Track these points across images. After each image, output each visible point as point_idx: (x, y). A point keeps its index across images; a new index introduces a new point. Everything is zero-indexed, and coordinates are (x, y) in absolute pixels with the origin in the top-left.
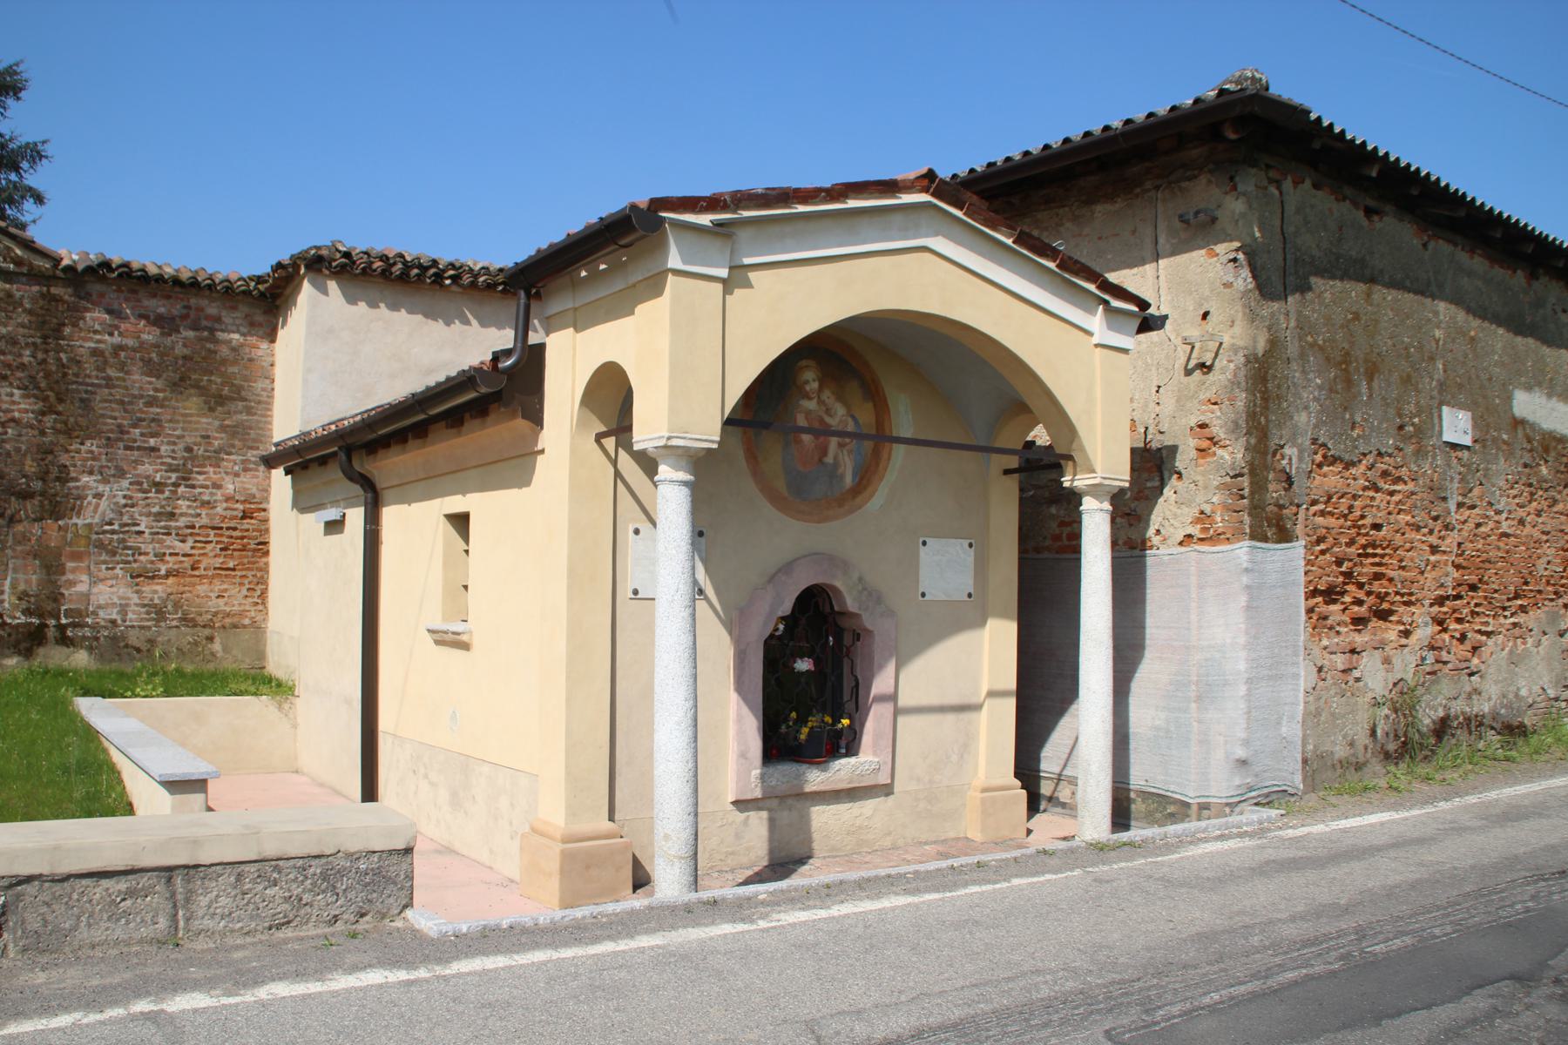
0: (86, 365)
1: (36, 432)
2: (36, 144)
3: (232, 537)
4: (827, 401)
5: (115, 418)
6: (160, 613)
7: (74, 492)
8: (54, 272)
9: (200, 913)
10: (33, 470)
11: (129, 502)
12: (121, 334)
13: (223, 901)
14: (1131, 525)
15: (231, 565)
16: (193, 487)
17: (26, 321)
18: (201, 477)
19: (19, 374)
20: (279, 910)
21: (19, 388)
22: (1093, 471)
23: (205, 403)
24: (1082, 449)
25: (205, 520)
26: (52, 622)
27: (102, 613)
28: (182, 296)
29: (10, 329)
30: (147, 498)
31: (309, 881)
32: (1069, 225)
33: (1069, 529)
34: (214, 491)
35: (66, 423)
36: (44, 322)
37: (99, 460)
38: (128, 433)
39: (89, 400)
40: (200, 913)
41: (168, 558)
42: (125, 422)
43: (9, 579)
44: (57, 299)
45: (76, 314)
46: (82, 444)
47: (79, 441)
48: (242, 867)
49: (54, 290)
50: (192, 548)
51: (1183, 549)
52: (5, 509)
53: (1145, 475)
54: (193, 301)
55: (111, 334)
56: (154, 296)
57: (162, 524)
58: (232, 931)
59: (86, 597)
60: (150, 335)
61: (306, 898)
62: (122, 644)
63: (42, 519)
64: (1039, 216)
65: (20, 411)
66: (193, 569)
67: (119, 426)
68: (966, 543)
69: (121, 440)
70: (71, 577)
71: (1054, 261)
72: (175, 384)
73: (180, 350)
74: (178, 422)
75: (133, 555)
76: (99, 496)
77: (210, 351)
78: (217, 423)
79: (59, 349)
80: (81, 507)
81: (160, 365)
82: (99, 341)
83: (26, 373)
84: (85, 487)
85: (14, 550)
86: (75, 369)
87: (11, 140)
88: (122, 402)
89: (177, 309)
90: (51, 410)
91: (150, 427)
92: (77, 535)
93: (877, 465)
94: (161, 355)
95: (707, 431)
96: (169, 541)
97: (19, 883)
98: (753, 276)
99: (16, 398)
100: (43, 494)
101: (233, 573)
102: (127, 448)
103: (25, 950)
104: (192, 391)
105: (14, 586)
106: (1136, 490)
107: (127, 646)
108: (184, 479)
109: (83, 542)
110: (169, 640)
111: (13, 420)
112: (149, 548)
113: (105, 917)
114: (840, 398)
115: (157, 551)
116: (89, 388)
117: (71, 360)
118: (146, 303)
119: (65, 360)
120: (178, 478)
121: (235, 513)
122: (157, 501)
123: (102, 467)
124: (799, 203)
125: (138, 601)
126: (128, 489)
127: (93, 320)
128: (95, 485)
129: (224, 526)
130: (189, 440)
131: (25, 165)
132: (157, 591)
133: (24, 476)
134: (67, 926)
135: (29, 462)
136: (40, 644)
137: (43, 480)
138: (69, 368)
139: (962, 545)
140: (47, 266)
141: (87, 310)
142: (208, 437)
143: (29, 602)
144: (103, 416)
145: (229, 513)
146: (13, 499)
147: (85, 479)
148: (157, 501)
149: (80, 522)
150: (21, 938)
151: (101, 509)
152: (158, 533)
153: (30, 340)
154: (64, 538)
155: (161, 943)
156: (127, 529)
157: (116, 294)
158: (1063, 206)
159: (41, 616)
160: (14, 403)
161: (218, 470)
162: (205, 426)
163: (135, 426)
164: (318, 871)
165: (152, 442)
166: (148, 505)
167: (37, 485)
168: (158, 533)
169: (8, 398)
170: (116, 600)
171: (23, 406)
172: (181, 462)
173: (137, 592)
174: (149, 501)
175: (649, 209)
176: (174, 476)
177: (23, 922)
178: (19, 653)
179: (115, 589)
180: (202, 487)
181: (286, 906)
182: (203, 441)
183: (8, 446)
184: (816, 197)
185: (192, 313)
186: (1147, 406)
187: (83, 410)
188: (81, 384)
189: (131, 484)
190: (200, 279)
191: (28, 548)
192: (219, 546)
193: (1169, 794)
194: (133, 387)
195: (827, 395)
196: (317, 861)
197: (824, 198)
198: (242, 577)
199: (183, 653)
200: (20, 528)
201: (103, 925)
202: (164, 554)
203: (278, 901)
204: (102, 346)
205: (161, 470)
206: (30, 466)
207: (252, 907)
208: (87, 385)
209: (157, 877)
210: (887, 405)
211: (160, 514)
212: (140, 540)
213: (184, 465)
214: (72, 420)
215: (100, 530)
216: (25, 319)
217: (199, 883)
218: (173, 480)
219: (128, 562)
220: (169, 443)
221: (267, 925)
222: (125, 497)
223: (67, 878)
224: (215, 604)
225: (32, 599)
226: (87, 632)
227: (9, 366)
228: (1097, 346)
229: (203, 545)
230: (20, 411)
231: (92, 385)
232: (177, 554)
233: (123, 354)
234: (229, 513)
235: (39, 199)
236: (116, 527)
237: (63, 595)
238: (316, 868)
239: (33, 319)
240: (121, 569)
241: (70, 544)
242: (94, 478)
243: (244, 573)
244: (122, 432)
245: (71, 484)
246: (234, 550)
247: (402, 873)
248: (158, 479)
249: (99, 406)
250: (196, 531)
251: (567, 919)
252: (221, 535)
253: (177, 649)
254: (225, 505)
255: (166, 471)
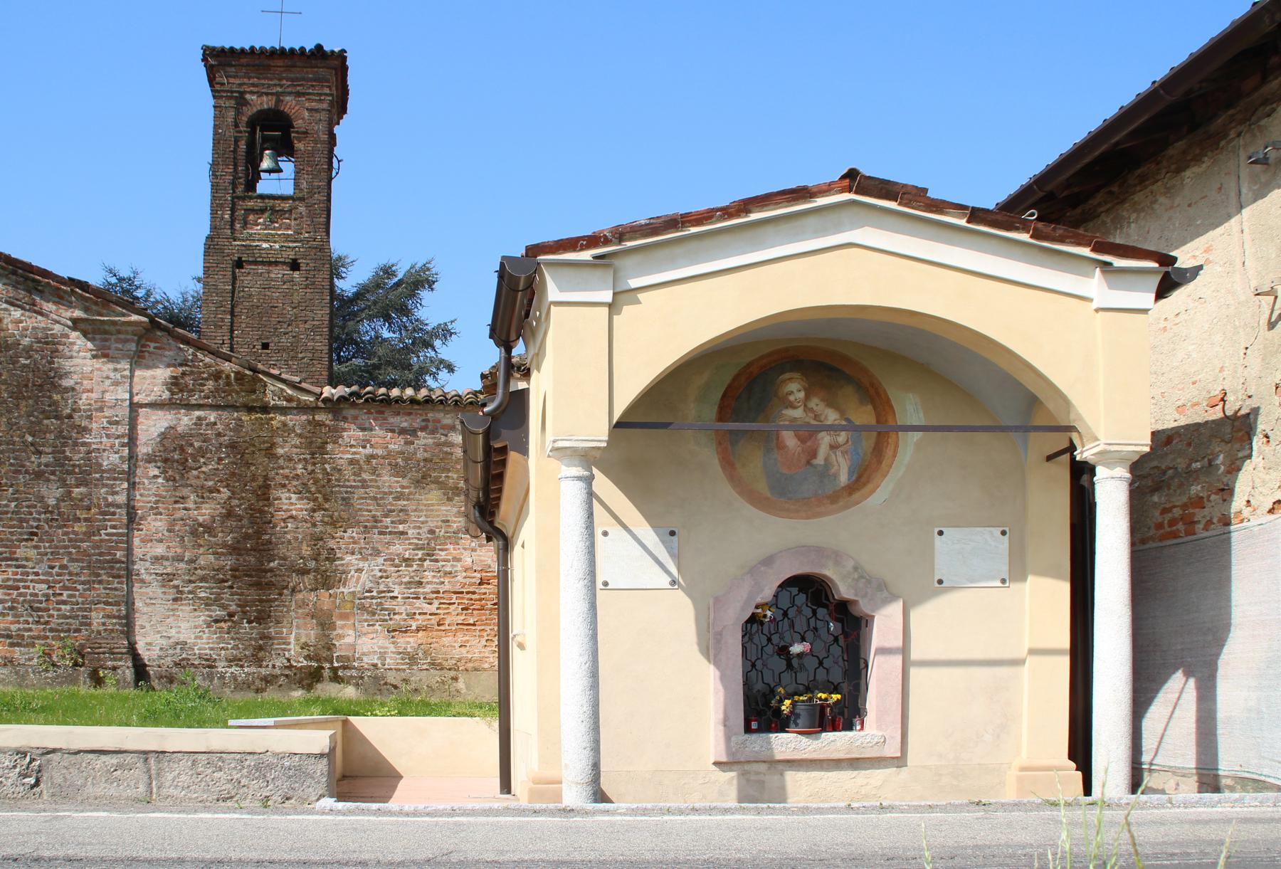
0: (345, 472)
1: (309, 525)
2: (446, 324)
3: (471, 599)
4: (815, 408)
5: (370, 511)
6: (413, 659)
7: (340, 568)
8: (317, 404)
9: (167, 784)
10: (308, 553)
11: (384, 574)
12: (372, 446)
13: (183, 778)
14: (1225, 500)
15: (471, 622)
16: (437, 561)
17: (298, 443)
18: (443, 553)
19: (295, 483)
20: (224, 788)
21: (295, 493)
22: (1097, 439)
23: (444, 495)
24: (1080, 418)
25: (447, 587)
26: (327, 665)
27: (365, 659)
28: (420, 412)
29: (287, 449)
30: (398, 571)
31: (245, 770)
32: (1162, 200)
33: (1170, 515)
34: (455, 563)
35: (332, 517)
36: (311, 443)
37: (359, 543)
38: (381, 521)
39: (349, 498)
40: (167, 784)
41: (417, 617)
42: (379, 514)
43: (294, 633)
44: (320, 424)
45: (335, 433)
46: (345, 532)
47: (342, 529)
48: (197, 755)
49: (317, 417)
50: (438, 609)
51: (1272, 517)
52: (289, 582)
53: (1237, 446)
54: (430, 415)
55: (364, 447)
56: (398, 414)
57: (413, 590)
58: (190, 799)
59: (353, 646)
60: (396, 444)
61: (244, 781)
62: (382, 682)
63: (317, 590)
64: (1136, 198)
65: (296, 510)
66: (439, 625)
67: (374, 516)
68: (997, 531)
69: (376, 527)
70: (340, 632)
71: (1028, 232)
72: (418, 482)
73: (421, 455)
74: (422, 510)
75: (389, 614)
76: (359, 570)
77: (446, 453)
78: (455, 510)
79: (324, 462)
80: (346, 579)
81: (404, 467)
82: (355, 453)
83: (300, 481)
84: (348, 565)
85: (297, 613)
86: (337, 476)
87: (185, 300)
88: (375, 499)
89: (417, 423)
90: (320, 508)
91: (399, 516)
92: (344, 600)
93: (880, 462)
94: (406, 460)
95: (597, 432)
96: (418, 603)
97: (48, 753)
98: (641, 296)
99: (293, 500)
100: (316, 570)
101: (474, 628)
102: (381, 533)
103: (53, 795)
104: (433, 486)
105: (297, 639)
106: (1228, 463)
107: (386, 684)
108: (428, 555)
109: (349, 605)
110: (420, 680)
111: (291, 517)
112: (402, 609)
113: (103, 780)
114: (831, 404)
115: (408, 611)
116: (349, 489)
117: (334, 469)
118: (391, 420)
119: (329, 470)
120: (423, 554)
121: (474, 580)
122: (407, 573)
123: (361, 548)
124: (693, 226)
125: (394, 650)
126: (383, 565)
127: (348, 436)
128: (357, 562)
129: (465, 590)
130: (432, 524)
131: (437, 343)
132: (409, 642)
133: (301, 558)
134: (79, 783)
135: (304, 547)
136: (318, 681)
137: (315, 559)
138: (332, 475)
139: (991, 533)
140: (312, 399)
141: (344, 430)
142: (448, 521)
143: (309, 651)
144: (360, 509)
145: (468, 581)
146: (294, 575)
147: (348, 558)
148: (407, 573)
149: (346, 591)
150: (51, 788)
151: (361, 581)
152: (409, 598)
153: (302, 457)
154: (334, 602)
155: (139, 801)
156: (383, 595)
157: (366, 416)
158: (1157, 181)
159: (318, 661)
160: (292, 504)
161: (457, 546)
162: (445, 512)
163: (386, 516)
164: (252, 764)
165: (401, 527)
166: (400, 576)
167: (312, 564)
168: (409, 598)
169: (287, 501)
170: (376, 649)
171: (299, 506)
172: (426, 542)
173: (393, 643)
174: (401, 573)
175: (527, 255)
176: (420, 553)
177: (51, 778)
178: (303, 688)
179: (375, 641)
180: (444, 561)
181: (229, 786)
182: (443, 525)
183: (289, 537)
184: (711, 217)
185: (430, 425)
186: (1236, 372)
187: (345, 506)
188: (342, 487)
189: (385, 560)
190: (434, 397)
191: (307, 611)
192: (460, 607)
193: (1263, 778)
194: (383, 486)
195: (815, 403)
196: (251, 756)
197: (721, 216)
198: (481, 630)
199: (433, 690)
200: (300, 596)
201: (103, 785)
202: (415, 614)
203: (223, 781)
204: (357, 456)
205: (410, 549)
206: (306, 551)
207: (203, 784)
208: (347, 487)
209: (138, 757)
210: (891, 407)
211: (410, 583)
212: (395, 603)
213: (428, 544)
214: (336, 514)
215: (362, 596)
216: (297, 441)
217: (166, 764)
218: (420, 556)
219: (385, 620)
220: (415, 528)
221: (215, 797)
222: (380, 571)
223: (79, 752)
224: (458, 652)
225: (312, 649)
226: (354, 673)
227: (287, 477)
228: (1097, 310)
229: (447, 606)
230: (296, 510)
231: (351, 487)
232: (425, 614)
233: (374, 461)
234: (468, 581)
235: (450, 368)
236: (374, 594)
237: (335, 645)
238: (251, 761)
239: (303, 440)
240: (380, 625)
241: (339, 607)
242: (354, 557)
243: (483, 627)
244: (376, 521)
245: (337, 563)
246: (474, 609)
247: (319, 771)
248: (407, 556)
249: (357, 504)
250: (441, 595)
251: (429, 809)
252: (463, 598)
253: (427, 686)
254: (464, 574)
255: (413, 550)
